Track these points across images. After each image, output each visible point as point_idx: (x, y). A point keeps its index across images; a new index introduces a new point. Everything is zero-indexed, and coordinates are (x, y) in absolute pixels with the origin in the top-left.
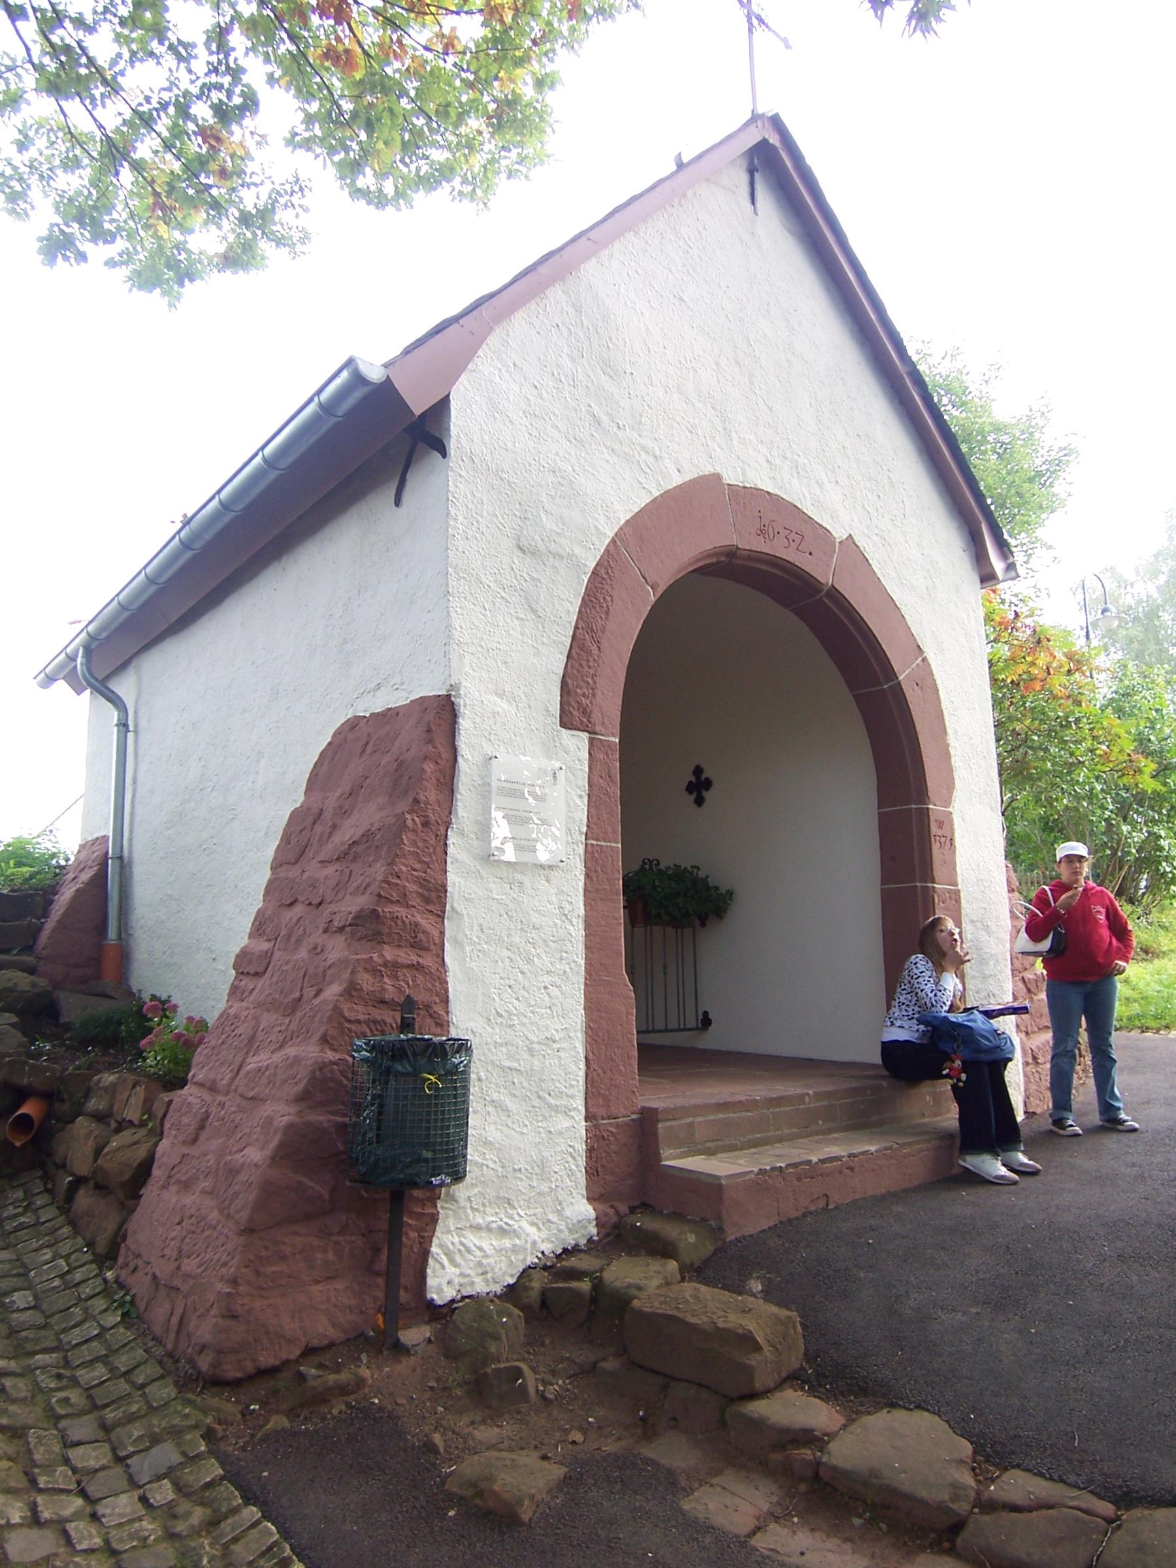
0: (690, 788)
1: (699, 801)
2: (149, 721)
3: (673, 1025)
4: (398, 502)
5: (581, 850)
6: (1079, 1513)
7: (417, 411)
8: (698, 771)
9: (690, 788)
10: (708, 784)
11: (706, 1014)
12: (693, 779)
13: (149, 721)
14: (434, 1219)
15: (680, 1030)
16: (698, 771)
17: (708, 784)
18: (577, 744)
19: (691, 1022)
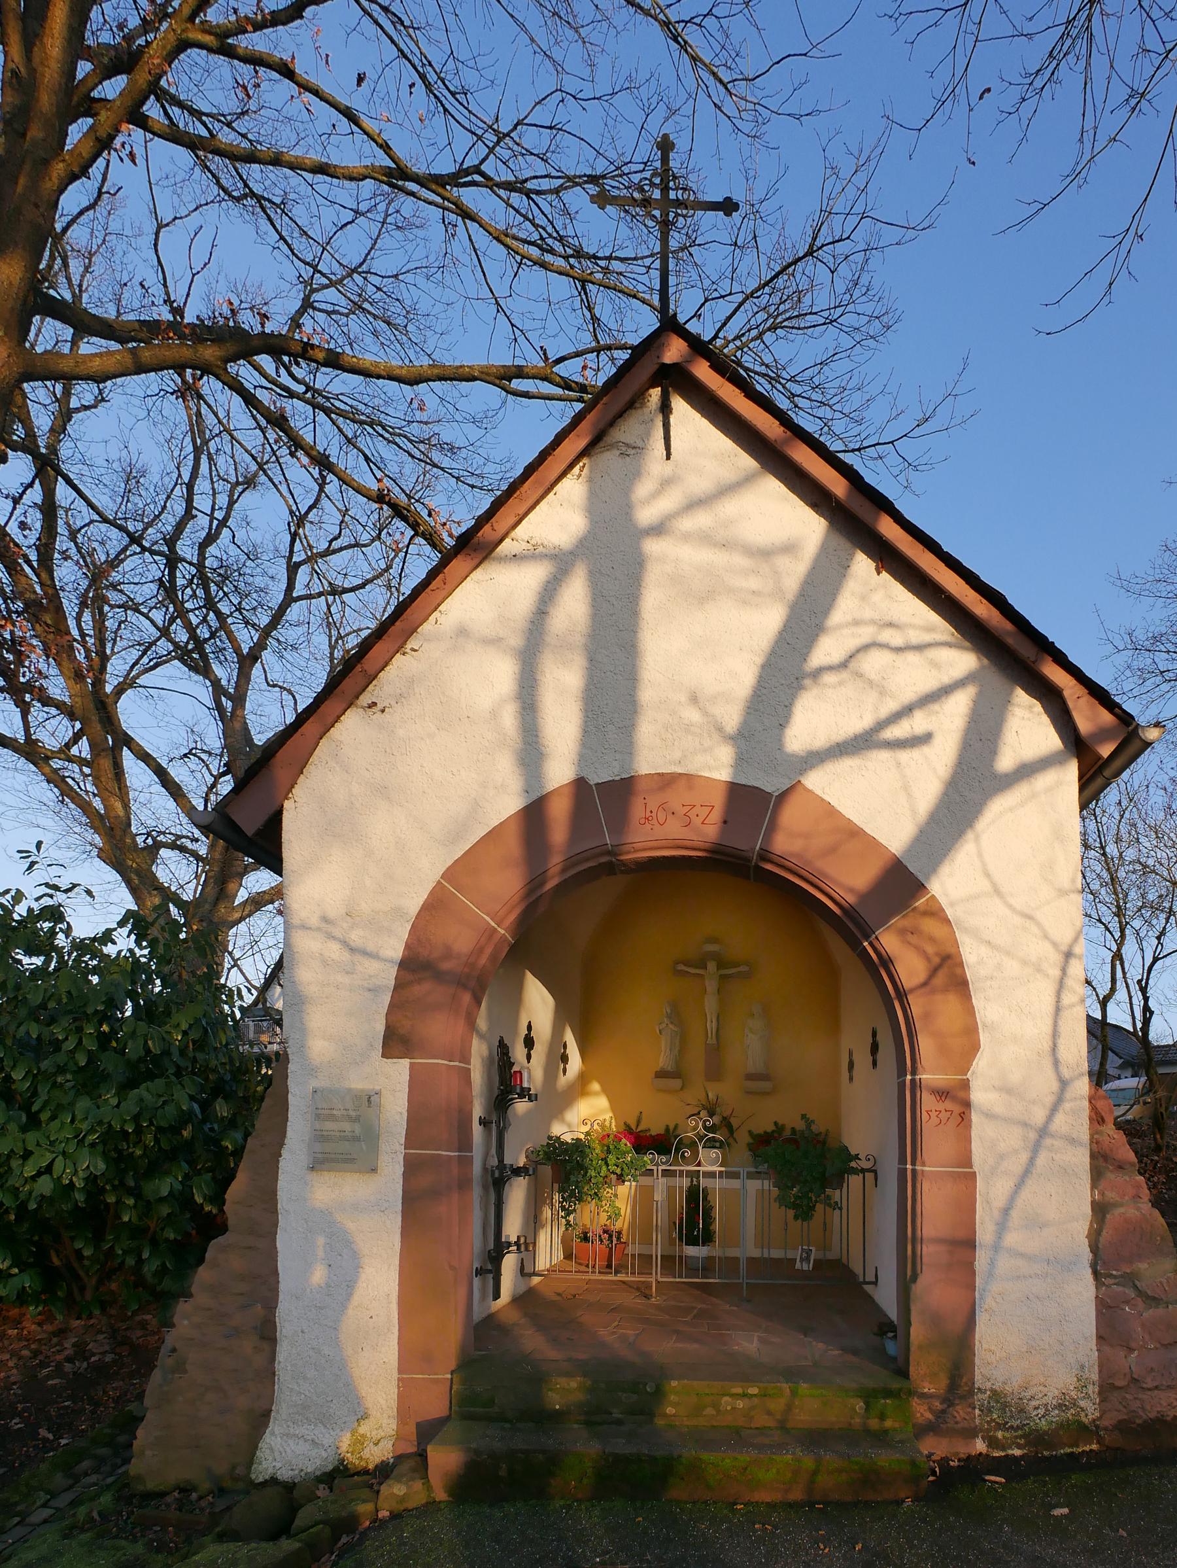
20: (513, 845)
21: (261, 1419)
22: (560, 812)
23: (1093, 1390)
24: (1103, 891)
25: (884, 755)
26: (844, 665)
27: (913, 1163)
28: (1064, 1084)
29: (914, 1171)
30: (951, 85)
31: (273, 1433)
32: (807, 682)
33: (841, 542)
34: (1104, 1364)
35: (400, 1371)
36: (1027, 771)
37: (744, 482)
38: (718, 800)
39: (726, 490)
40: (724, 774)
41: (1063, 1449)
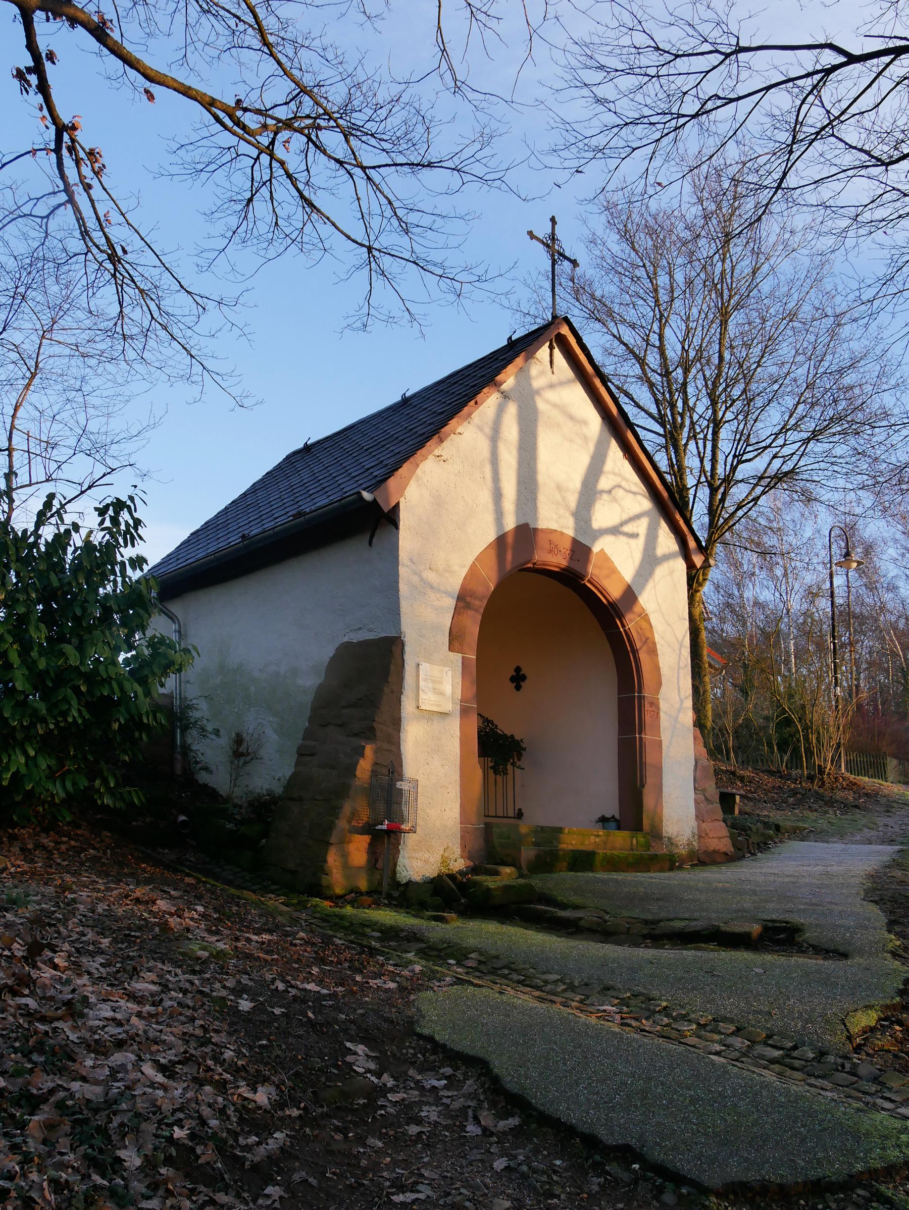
0: (513, 679)
1: (518, 688)
2: (608, 913)
3: (500, 813)
4: (370, 544)
5: (458, 707)
6: (476, 981)
7: (386, 511)
8: (518, 669)
9: (513, 679)
10: (524, 678)
11: (520, 810)
12: (514, 674)
13: (608, 913)
14: (399, 852)
15: (504, 817)
16: (518, 669)
17: (524, 678)
18: (457, 658)
19: (511, 814)
20: (493, 554)
21: (370, 845)
22: (510, 540)
23: (696, 837)
24: (629, 284)
25: (623, 539)
26: (610, 492)
27: (640, 733)
28: (682, 701)
29: (641, 738)
30: (608, 40)
31: (404, 857)
32: (598, 495)
33: (607, 434)
34: (699, 827)
35: (461, 823)
36: (667, 557)
37: (569, 382)
38: (568, 545)
39: (561, 384)
40: (571, 532)
41: (132, 656)
